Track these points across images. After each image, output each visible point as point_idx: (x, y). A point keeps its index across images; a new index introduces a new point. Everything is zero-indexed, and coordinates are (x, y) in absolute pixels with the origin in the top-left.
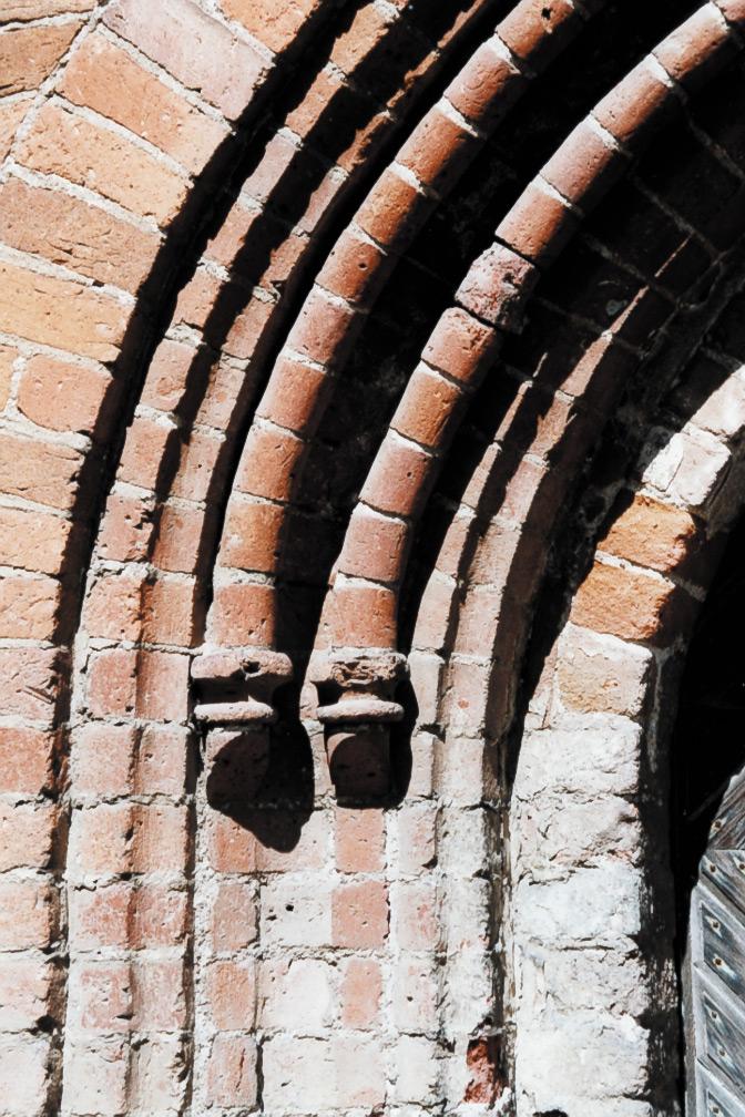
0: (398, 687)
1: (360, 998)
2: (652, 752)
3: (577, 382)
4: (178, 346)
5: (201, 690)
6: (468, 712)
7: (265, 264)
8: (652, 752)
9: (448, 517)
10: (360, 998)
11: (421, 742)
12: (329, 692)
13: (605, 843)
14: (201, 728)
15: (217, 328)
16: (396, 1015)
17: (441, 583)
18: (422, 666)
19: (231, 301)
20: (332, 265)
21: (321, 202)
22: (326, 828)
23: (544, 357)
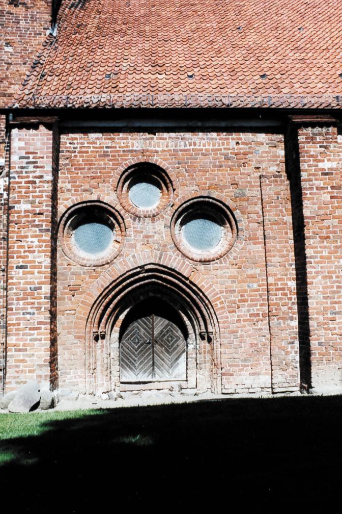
0: (105, 332)
1: (102, 351)
2: (223, 124)
3: (117, 311)
4: (93, 311)
5: (93, 333)
6: (109, 333)
7: (123, 283)
8: (223, 124)
9: (136, 283)
10: (102, 351)
11: (106, 335)
12: (101, 332)
13: (116, 341)
14: (93, 335)
15: (95, 310)
16: (104, 352)
17: (108, 325)
18: (107, 330)
19: (96, 308)
20: (102, 305)
21: (102, 302)
22: (100, 341)
23: (191, 211)
